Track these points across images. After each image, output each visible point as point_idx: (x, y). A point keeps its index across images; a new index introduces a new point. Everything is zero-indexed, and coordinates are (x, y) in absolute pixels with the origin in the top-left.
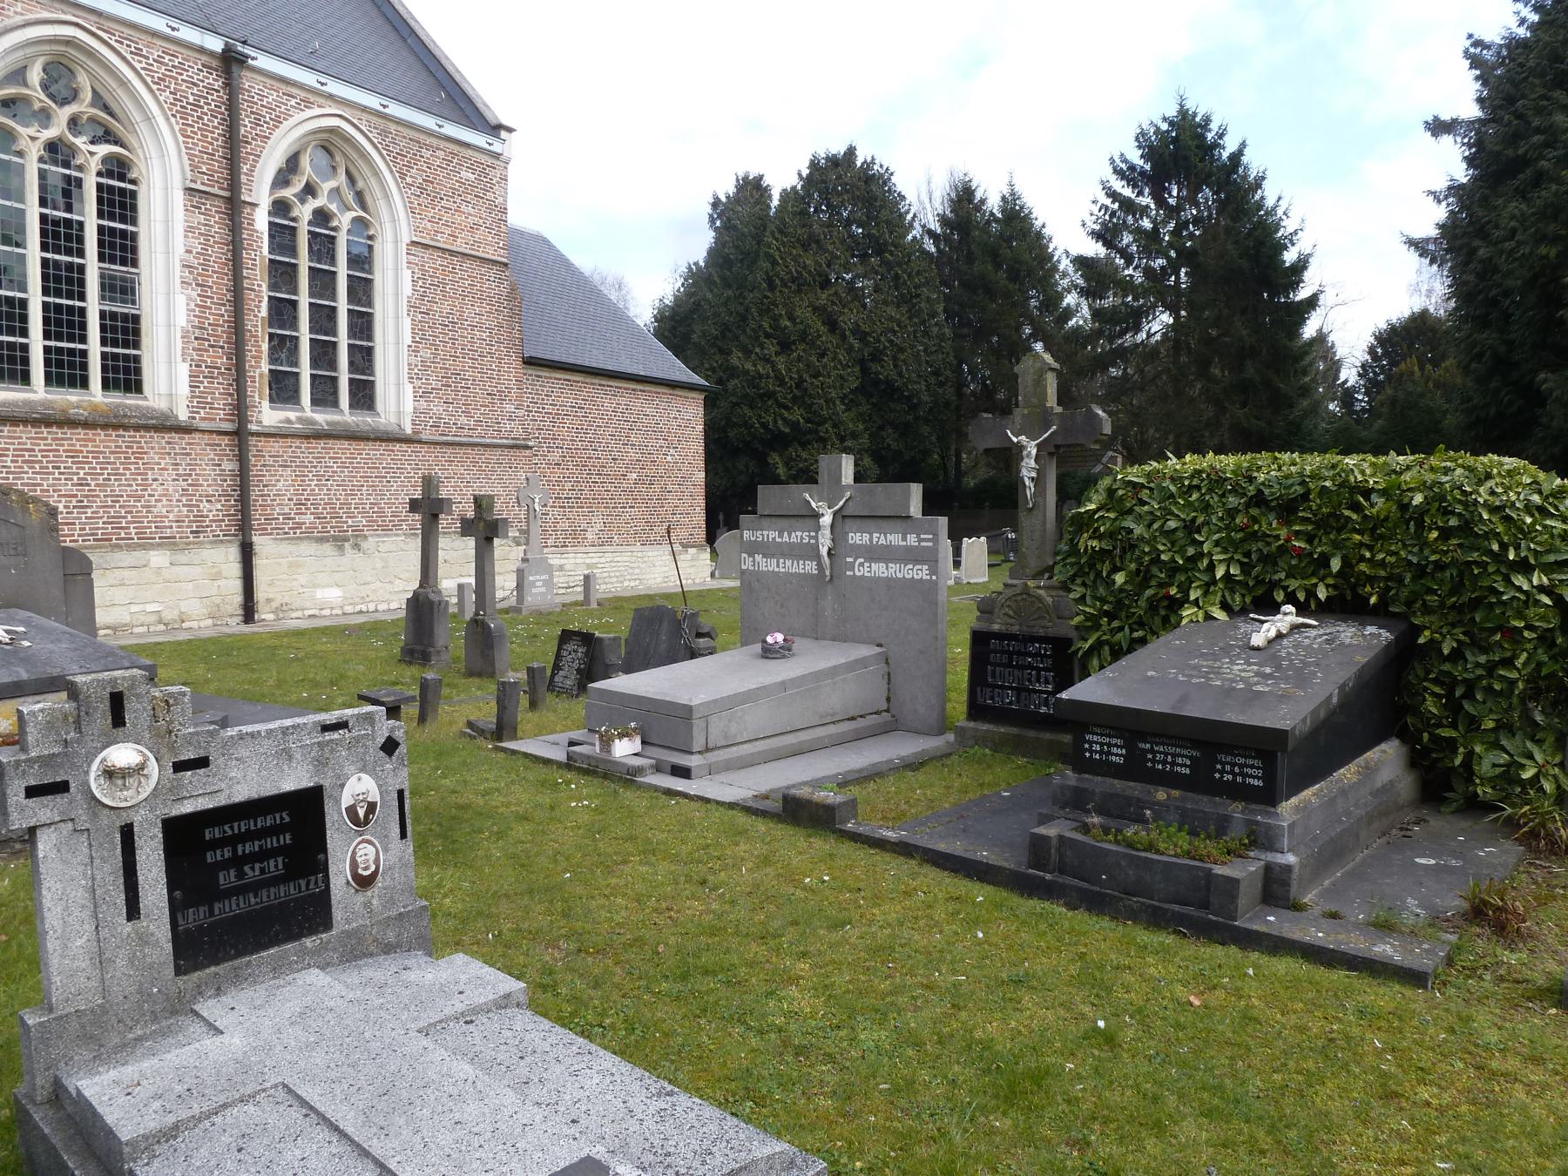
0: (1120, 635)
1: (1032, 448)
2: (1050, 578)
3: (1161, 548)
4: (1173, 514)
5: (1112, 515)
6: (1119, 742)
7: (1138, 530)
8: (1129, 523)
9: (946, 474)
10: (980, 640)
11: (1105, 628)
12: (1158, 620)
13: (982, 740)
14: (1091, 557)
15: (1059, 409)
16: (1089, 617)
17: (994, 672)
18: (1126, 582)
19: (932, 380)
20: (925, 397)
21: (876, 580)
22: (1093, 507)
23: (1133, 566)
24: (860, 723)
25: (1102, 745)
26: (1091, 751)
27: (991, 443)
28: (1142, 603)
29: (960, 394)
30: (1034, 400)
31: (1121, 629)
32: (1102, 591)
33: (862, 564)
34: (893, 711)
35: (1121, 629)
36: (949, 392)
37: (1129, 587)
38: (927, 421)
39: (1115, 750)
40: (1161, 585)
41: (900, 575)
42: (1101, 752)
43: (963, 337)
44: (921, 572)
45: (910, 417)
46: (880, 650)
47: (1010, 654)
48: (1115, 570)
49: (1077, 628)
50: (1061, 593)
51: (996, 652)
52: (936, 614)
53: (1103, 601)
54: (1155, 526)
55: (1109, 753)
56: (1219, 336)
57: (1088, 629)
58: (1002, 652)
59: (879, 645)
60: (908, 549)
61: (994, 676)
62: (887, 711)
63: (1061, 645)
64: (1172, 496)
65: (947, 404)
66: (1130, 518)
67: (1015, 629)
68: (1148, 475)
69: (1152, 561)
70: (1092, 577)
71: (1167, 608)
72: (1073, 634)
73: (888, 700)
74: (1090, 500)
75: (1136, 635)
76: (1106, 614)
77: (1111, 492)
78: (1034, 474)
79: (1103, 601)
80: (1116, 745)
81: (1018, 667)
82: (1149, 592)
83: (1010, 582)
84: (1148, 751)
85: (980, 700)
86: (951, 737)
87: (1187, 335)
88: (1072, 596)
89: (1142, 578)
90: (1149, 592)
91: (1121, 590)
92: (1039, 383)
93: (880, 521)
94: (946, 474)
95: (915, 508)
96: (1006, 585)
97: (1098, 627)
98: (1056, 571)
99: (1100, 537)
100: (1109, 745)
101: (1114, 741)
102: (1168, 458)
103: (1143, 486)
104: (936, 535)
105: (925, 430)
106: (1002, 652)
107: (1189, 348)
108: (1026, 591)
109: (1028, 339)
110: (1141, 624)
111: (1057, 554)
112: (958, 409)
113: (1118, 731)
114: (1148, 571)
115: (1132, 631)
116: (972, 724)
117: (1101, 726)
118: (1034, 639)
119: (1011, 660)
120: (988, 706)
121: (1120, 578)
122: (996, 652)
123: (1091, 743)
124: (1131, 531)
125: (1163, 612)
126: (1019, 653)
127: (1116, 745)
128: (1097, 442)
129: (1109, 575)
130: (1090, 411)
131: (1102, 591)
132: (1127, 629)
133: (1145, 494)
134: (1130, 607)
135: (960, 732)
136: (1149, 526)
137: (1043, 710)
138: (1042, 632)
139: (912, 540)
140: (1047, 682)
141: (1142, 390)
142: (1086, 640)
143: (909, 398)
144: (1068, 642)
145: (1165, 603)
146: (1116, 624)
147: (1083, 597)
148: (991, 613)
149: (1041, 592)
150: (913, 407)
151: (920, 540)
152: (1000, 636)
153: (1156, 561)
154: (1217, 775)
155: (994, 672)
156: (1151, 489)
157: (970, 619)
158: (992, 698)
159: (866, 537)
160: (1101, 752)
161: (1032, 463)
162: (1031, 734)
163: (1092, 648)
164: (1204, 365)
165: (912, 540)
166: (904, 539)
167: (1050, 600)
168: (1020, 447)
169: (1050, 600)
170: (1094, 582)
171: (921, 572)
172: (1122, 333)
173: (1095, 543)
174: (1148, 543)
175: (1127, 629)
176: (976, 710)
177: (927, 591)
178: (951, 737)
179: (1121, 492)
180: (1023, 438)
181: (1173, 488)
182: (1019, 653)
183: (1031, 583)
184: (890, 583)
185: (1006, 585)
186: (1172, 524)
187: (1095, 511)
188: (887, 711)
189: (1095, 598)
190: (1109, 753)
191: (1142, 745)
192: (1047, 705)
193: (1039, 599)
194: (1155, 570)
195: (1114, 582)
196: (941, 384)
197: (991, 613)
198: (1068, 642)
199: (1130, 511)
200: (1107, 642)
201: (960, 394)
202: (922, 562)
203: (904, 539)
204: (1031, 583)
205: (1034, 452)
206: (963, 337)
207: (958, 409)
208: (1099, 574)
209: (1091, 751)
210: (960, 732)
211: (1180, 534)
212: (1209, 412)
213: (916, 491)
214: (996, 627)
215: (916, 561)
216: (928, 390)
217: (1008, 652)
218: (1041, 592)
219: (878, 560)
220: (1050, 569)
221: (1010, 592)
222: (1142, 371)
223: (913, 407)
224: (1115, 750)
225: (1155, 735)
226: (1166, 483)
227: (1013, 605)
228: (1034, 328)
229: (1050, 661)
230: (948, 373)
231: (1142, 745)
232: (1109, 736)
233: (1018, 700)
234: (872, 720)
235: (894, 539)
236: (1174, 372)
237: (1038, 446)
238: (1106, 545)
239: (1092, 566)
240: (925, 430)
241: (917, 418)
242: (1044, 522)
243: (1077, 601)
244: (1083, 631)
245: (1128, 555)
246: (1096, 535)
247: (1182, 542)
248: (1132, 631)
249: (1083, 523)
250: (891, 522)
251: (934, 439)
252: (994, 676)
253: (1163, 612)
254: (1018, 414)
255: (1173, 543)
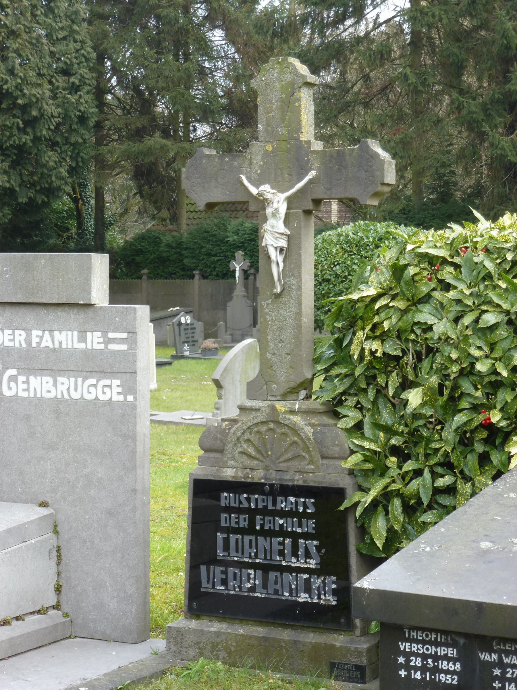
0: (415, 484)
1: (278, 202)
2: (308, 397)
3: (477, 353)
4: (490, 302)
5: (401, 304)
6: (451, 652)
7: (441, 327)
8: (425, 315)
9: (80, 225)
10: (204, 490)
11: (394, 472)
12: (472, 460)
13: (211, 649)
14: (370, 366)
15: (318, 146)
16: (371, 456)
17: (226, 541)
18: (423, 404)
19: (61, 81)
20: (51, 108)
21: (39, 402)
22: (372, 292)
23: (434, 380)
24: (17, 629)
25: (424, 657)
26: (408, 667)
27: (218, 195)
28: (449, 434)
29: (101, 104)
30: (282, 131)
31: (418, 473)
32: (386, 417)
33: (13, 379)
34: (65, 608)
35: (418, 473)
36: (85, 101)
37: (428, 411)
38: (53, 145)
39: (444, 665)
40: (475, 408)
41: (75, 395)
42: (424, 669)
43: (103, 17)
44: (109, 390)
45: (27, 139)
46: (44, 511)
47: (252, 513)
48: (406, 385)
49: (351, 472)
50: (327, 420)
51: (228, 510)
52: (133, 454)
53: (389, 431)
54: (467, 320)
55: (436, 670)
56: (476, 28)
57: (366, 473)
58: (239, 511)
59: (44, 504)
60: (88, 355)
61: (226, 547)
62: (56, 607)
63: (328, 498)
64: (489, 276)
65: (83, 119)
66: (426, 308)
67: (258, 476)
68: (453, 246)
69: (461, 373)
70: (371, 394)
71: (486, 441)
72: (346, 482)
73: (58, 589)
74: (365, 282)
75: (441, 482)
76: (395, 451)
77: (398, 271)
78: (283, 243)
79: (389, 431)
80: (446, 657)
81: (265, 533)
82: (460, 419)
83: (249, 404)
84: (494, 665)
85: (206, 586)
86: (160, 644)
87: (430, 26)
88: (343, 424)
89: (450, 399)
90: (460, 419)
91: (415, 416)
92: (289, 104)
93: (42, 312)
94: (80, 225)
95: (99, 289)
96: (242, 409)
97: (384, 471)
98: (316, 386)
99: (383, 337)
100: (436, 658)
101: (443, 651)
102: (475, 221)
103: (444, 261)
104: (133, 333)
105: (50, 158)
106: (239, 511)
107: (432, 45)
108: (274, 418)
109: (201, 25)
110: (448, 466)
111: (317, 361)
112: (98, 126)
113: (448, 636)
114: (455, 387)
115: (435, 475)
116: (193, 624)
117: (423, 630)
118: (286, 490)
119: (252, 522)
120: (220, 595)
121: (414, 398)
122: (228, 510)
123: (408, 655)
124: (430, 328)
125: (480, 448)
126: (265, 512)
127: (446, 657)
128: (376, 194)
129: (396, 395)
130: (367, 149)
131: (386, 417)
132: (427, 474)
133: (447, 274)
134: (429, 440)
135: (175, 637)
136: (457, 320)
137: (303, 598)
138: (298, 480)
139: (95, 340)
140: (308, 555)
141: (367, 105)
142: (366, 491)
143: (25, 109)
144: (339, 494)
145: (484, 434)
146: (409, 466)
147: (359, 426)
148: (221, 451)
149: (297, 419)
150: (32, 123)
151: (108, 341)
152: (235, 487)
153: (468, 372)
154: (403, 673)
155: (226, 541)
156: (457, 266)
157: (188, 461)
158: (224, 582)
159: (20, 336)
160: (424, 669)
161: (281, 227)
162: (285, 635)
163: (375, 504)
164: (454, 70)
165: (95, 340)
166: (83, 339)
167: (309, 431)
168: (262, 203)
169: (309, 431)
170: (374, 403)
171: (109, 390)
172: (340, 19)
173: (375, 345)
174: (456, 346)
175: (427, 474)
176: (200, 601)
177: (120, 418)
178: (160, 644)
179: (412, 271)
180: (266, 188)
181: (490, 265)
182: (265, 512)
183: (281, 406)
184: (59, 407)
185: (242, 409)
186: (490, 318)
187: (374, 300)
188: (56, 607)
189: (377, 426)
190: (436, 670)
191: (485, 657)
192: (308, 590)
193: (295, 430)
194: (466, 386)
195: (405, 403)
196: (75, 89)
197: (221, 451)
198: (339, 494)
199: (427, 298)
200: (398, 494)
201: (101, 104)
202: (111, 374)
203: (83, 339)
204: (281, 406)
205: (283, 209)
206: (103, 17)
207: (98, 126)
208: (381, 392)
209: (408, 667)
210: (175, 637)
211: (503, 332)
212: (460, 140)
213: (100, 264)
214: (229, 473)
215: (103, 373)
216: (54, 97)
217: (249, 511)
218: (297, 419)
219: (40, 371)
220: (307, 384)
221: (249, 419)
222: (366, 78)
223: (32, 123)
224: (444, 665)
225: (504, 640)
226: (480, 257)
227: (255, 439)
228: (210, 9)
229: (312, 523)
230: (84, 71)
231: (485, 657)
232: (436, 644)
233: (265, 585)
234: (34, 623)
235: (66, 339)
236: (412, 79)
237: (290, 200)
238: (392, 348)
239: (371, 379)
240: (50, 158)
241: (36, 140)
242: (299, 314)
243: (349, 431)
244: (361, 477)
245: (425, 364)
246: (377, 333)
247: (505, 345)
248: (435, 475)
249: (354, 317)
250: (62, 314)
251: (63, 171)
252: (226, 547)
253: (480, 448)
254: (258, 151)
255: (492, 346)
